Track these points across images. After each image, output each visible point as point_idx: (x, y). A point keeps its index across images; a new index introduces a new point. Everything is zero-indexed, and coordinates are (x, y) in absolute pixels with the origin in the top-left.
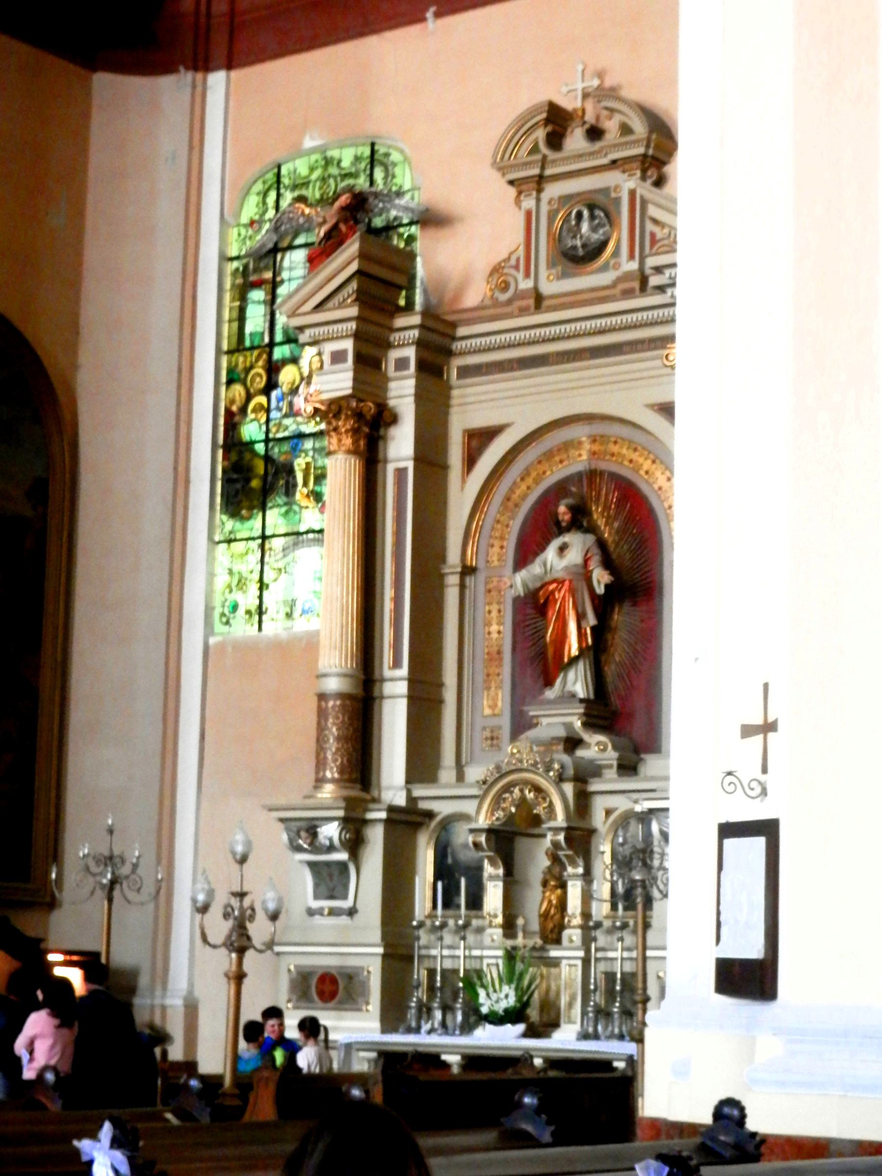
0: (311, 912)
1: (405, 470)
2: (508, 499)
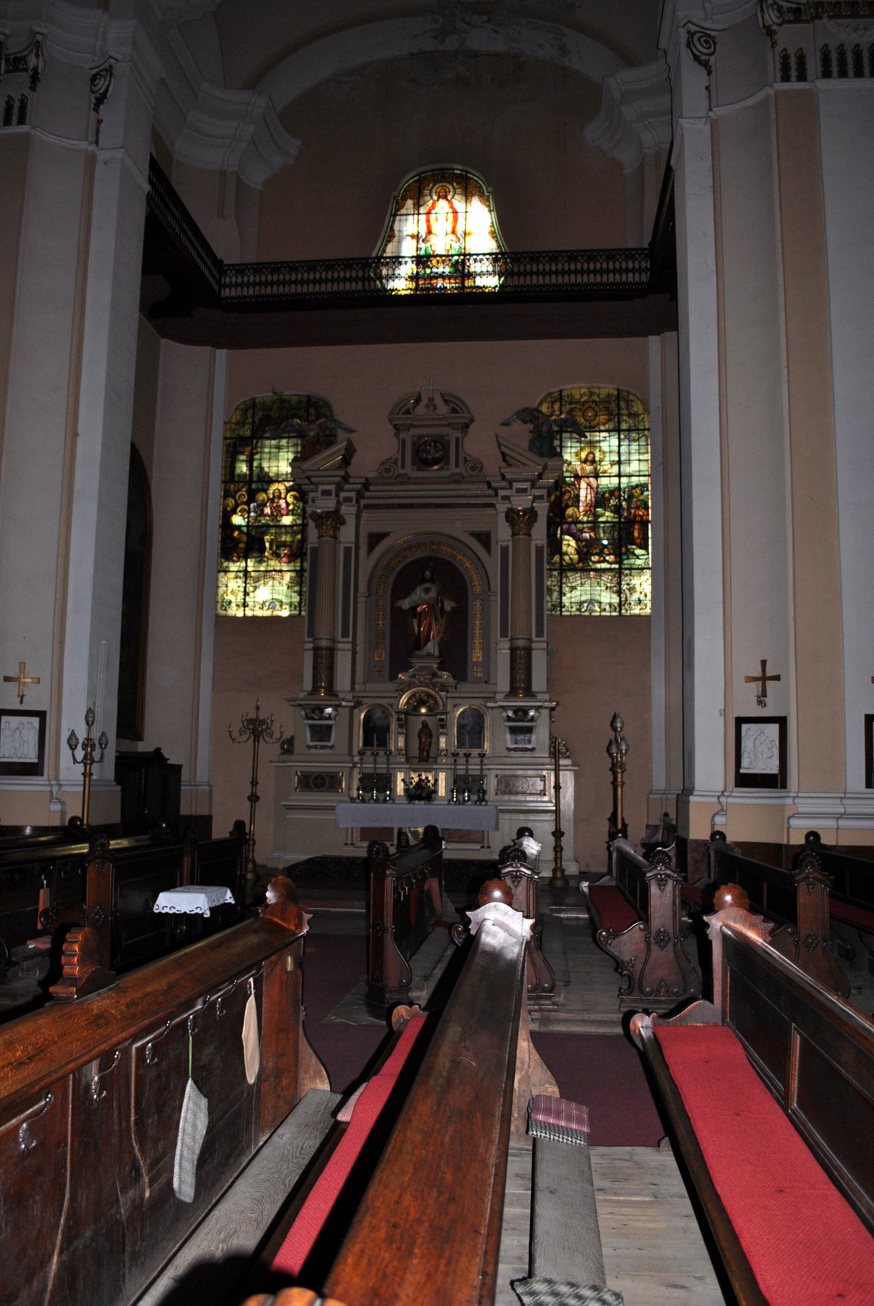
0: (309, 747)
1: (507, 547)
2: (388, 565)
